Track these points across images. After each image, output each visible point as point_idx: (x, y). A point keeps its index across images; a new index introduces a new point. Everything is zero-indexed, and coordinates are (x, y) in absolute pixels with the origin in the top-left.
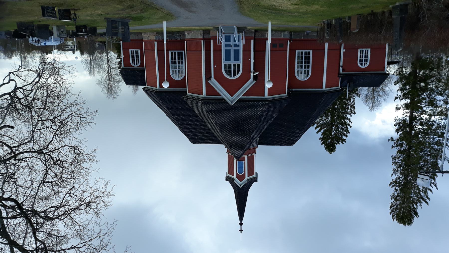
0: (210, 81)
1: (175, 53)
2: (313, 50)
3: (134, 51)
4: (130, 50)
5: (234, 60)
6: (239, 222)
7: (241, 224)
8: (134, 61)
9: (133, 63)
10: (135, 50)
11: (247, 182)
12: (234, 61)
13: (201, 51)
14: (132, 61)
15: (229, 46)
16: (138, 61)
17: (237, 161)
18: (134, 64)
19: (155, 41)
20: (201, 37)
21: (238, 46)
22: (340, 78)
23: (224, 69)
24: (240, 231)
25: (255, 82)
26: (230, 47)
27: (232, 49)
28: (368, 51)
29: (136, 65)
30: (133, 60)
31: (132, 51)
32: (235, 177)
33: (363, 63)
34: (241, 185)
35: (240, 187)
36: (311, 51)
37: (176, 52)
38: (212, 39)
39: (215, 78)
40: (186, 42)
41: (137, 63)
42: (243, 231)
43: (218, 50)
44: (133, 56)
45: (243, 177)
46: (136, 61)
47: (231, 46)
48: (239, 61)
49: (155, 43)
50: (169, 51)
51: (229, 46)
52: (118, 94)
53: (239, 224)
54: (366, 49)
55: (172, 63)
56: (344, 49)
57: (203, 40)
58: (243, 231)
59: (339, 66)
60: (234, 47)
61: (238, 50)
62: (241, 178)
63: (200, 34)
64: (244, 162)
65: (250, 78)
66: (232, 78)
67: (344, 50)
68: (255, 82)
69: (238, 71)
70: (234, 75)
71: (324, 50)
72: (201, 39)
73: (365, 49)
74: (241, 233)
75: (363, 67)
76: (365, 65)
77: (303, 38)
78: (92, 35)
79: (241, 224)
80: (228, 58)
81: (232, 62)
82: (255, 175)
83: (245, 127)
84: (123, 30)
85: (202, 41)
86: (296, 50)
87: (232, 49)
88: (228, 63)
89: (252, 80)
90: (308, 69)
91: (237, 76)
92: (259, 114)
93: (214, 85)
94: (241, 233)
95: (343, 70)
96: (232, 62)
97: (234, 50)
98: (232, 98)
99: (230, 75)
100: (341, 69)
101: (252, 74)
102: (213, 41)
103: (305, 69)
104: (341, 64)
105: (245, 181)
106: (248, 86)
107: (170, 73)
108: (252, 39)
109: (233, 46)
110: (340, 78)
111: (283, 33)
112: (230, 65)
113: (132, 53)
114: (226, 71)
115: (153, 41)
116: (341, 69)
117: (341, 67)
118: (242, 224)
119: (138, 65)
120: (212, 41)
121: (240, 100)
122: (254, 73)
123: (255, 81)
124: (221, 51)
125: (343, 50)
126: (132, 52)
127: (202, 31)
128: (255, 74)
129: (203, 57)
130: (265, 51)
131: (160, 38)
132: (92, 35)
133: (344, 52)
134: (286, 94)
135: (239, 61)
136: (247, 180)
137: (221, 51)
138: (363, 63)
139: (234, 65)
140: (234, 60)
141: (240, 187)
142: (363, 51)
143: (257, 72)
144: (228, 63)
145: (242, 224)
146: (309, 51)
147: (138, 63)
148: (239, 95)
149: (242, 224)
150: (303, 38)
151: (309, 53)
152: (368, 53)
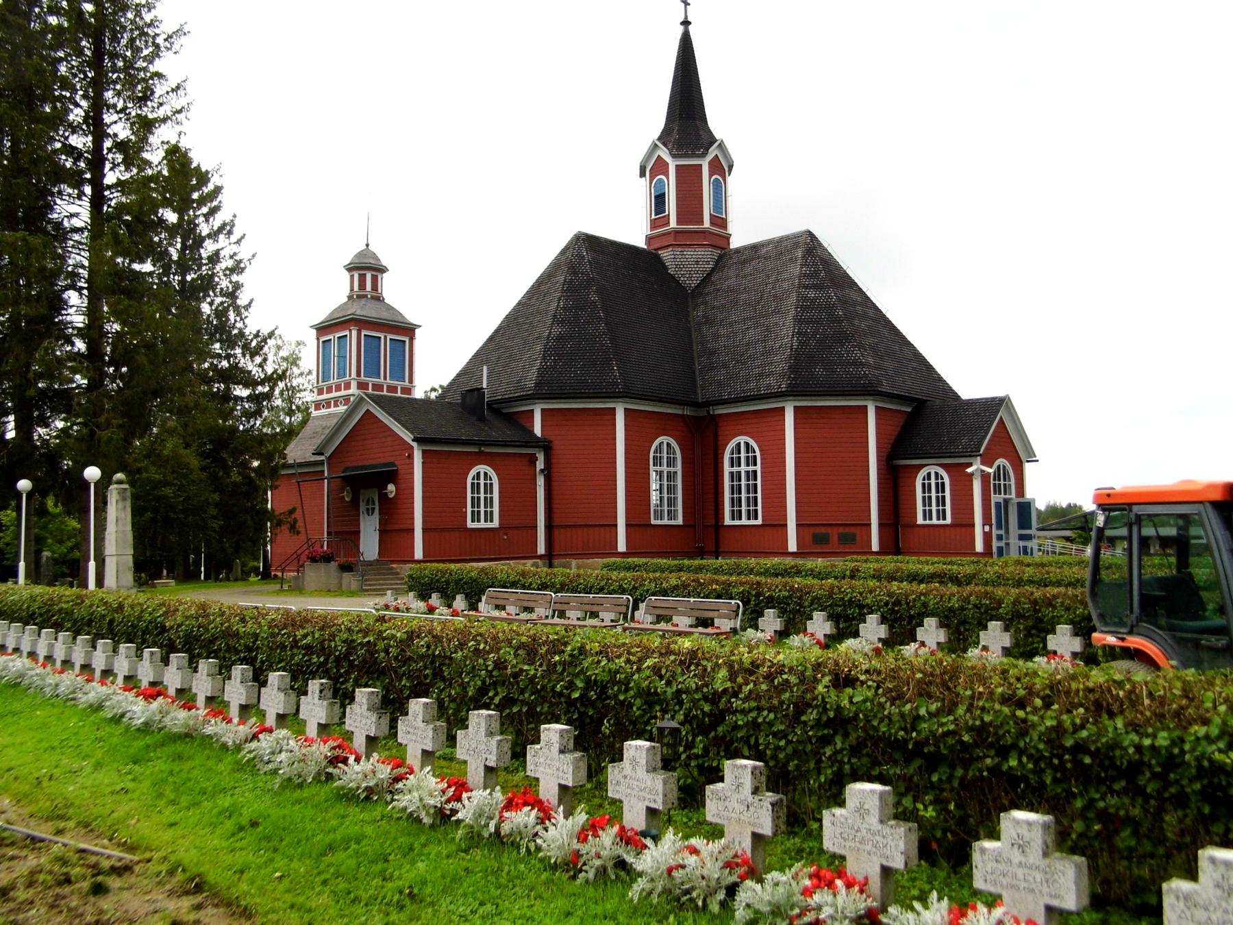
2: (915, 526)
3: (938, 519)
6: (690, 27)
7: (686, 23)
8: (937, 484)
9: (942, 478)
14: (943, 484)
18: (937, 474)
21: (1022, 537)
29: (933, 470)
30: (941, 487)
31: (944, 518)
33: (933, 481)
41: (929, 478)
52: (192, 404)
53: (689, 23)
59: (548, 473)
69: (656, 452)
75: (482, 468)
79: (686, 23)
86: (501, 528)
90: (669, 469)
95: (533, 460)
100: (540, 465)
104: (541, 481)
118: (682, 23)
119: (922, 473)
126: (753, 515)
137: (798, 525)
138: (933, 481)
139: (747, 473)
145: (682, 23)
147: (473, 479)
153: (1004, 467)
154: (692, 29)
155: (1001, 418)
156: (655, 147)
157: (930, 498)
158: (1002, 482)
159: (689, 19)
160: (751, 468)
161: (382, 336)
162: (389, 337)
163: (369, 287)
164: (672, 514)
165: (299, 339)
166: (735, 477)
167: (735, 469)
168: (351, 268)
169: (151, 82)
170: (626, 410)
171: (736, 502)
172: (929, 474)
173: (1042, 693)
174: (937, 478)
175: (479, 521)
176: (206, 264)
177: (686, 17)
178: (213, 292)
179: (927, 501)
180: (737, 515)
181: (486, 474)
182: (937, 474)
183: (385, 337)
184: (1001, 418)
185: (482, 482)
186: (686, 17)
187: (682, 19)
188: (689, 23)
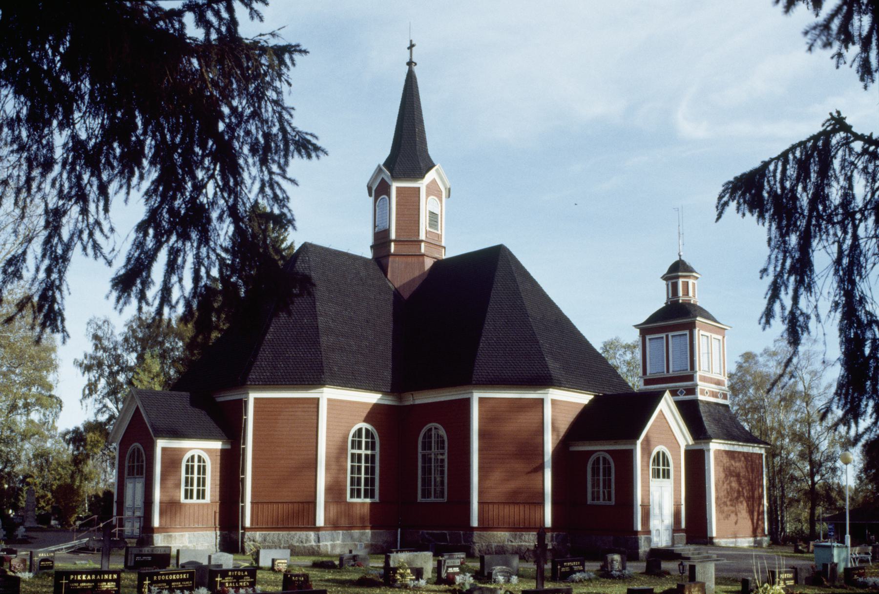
3: (198, 498)
7: (410, 63)
69: (424, 437)
72: (251, 529)
147: (188, 461)
153: (664, 454)
154: (416, 70)
155: (661, 411)
156: (379, 170)
157: (198, 485)
158: (661, 467)
159: (414, 60)
160: (356, 451)
161: (664, 335)
162: (670, 334)
163: (681, 293)
166: (426, 459)
167: (356, 451)
168: (666, 278)
171: (426, 482)
173: (168, 587)
175: (191, 498)
177: (411, 59)
178: (243, 223)
179: (595, 484)
180: (426, 494)
181: (199, 457)
183: (667, 337)
184: (661, 411)
185: (196, 464)
186: (411, 59)
187: (408, 60)
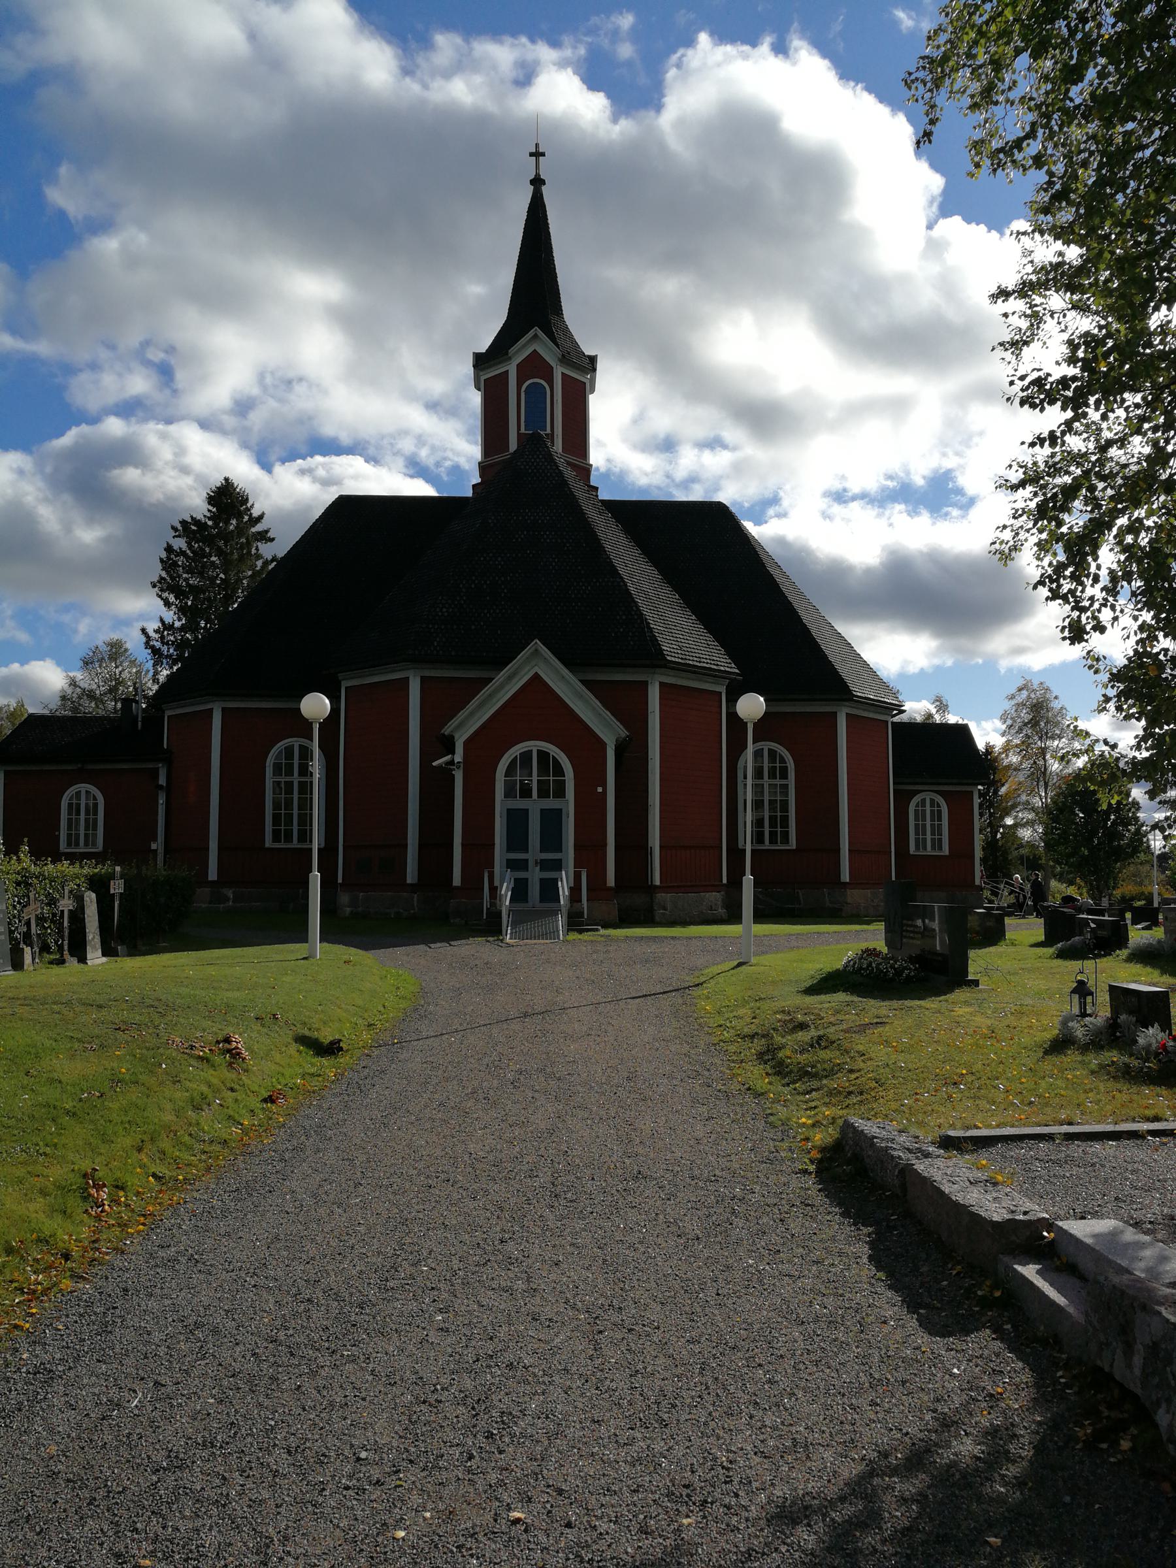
0: (621, 732)
1: (773, 840)
4: (946, 851)
5: (527, 811)
7: (537, 182)
8: (932, 812)
9: (939, 806)
10: (929, 851)
11: (512, 351)
12: (560, 807)
13: (661, 847)
14: (940, 812)
15: (545, 865)
16: (916, 811)
17: (548, 431)
18: (932, 801)
19: (845, 884)
20: (660, 896)
22: (165, 747)
23: (566, 778)
24: (543, 154)
25: (447, 730)
26: (541, 860)
27: (534, 852)
28: (69, 844)
29: (928, 796)
31: (940, 848)
32: (559, 372)
34: (536, 336)
35: (536, 330)
36: (268, 843)
37: (771, 842)
38: (610, 889)
39: (603, 745)
40: (725, 881)
41: (924, 805)
42: (531, 155)
43: (590, 850)
44: (936, 830)
45: (524, 371)
46: (924, 812)
47: (536, 863)
48: (508, 810)
49: (845, 877)
50: (794, 847)
51: (545, 865)
53: (543, 182)
54: (77, 850)
55: (785, 805)
56: (156, 850)
57: (656, 887)
58: (531, 155)
59: (169, 789)
60: (527, 860)
61: (510, 848)
62: (535, 367)
63: (666, 910)
64: (523, 430)
65: (466, 744)
66: (534, 746)
67: (154, 846)
68: (447, 730)
69: (510, 771)
70: (526, 757)
71: (838, 850)
73: (81, 850)
74: (537, 145)
75: (83, 787)
76: (78, 794)
77: (301, 891)
78: (1065, 910)
79: (537, 182)
80: (552, 819)
81: (535, 806)
82: (483, 378)
83: (499, 559)
84: (907, 931)
85: (657, 882)
86: (798, 850)
87: (534, 852)
88: (551, 803)
89: (456, 736)
91: (518, 753)
92: (444, 610)
93: (605, 719)
94: (537, 145)
95: (155, 774)
96: (535, 806)
97: (525, 849)
98: (536, 669)
99: (543, 756)
100: (162, 781)
101: (458, 758)
102: (842, 877)
103: (288, 779)
105: (520, 353)
106: (472, 714)
107: (793, 767)
108: (457, 888)
109: (531, 864)
110: (165, 747)
111: (360, 909)
112: (544, 793)
113: (940, 840)
114: (559, 771)
115: (855, 883)
116: (162, 781)
117: (162, 786)
118: (532, 182)
120: (611, 881)
121: (501, 661)
122: (452, 762)
123: (443, 735)
124: (577, 847)
125: (157, 845)
126: (938, 844)
127: (657, 919)
128: (448, 758)
129: (654, 825)
130: (421, 846)
131: (829, 894)
132: (1065, 910)
133: (155, 839)
134: (344, 684)
135: (508, 810)
136: (510, 358)
139: (526, 792)
140: (527, 811)
141: (536, 330)
142: (86, 844)
143: (440, 766)
144: (551, 803)
146: (277, 845)
147: (917, 806)
148: (510, 678)
149: (532, 182)
150: (301, 891)
151: (276, 837)
152: (69, 836)
164: (938, 844)
165: (1066, 706)
169: (1064, 529)
170: (223, 709)
172: (924, 801)
174: (932, 805)
176: (245, 577)
182: (932, 801)
188: (543, 182)
